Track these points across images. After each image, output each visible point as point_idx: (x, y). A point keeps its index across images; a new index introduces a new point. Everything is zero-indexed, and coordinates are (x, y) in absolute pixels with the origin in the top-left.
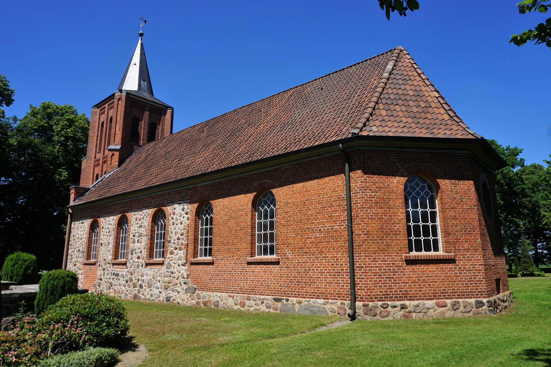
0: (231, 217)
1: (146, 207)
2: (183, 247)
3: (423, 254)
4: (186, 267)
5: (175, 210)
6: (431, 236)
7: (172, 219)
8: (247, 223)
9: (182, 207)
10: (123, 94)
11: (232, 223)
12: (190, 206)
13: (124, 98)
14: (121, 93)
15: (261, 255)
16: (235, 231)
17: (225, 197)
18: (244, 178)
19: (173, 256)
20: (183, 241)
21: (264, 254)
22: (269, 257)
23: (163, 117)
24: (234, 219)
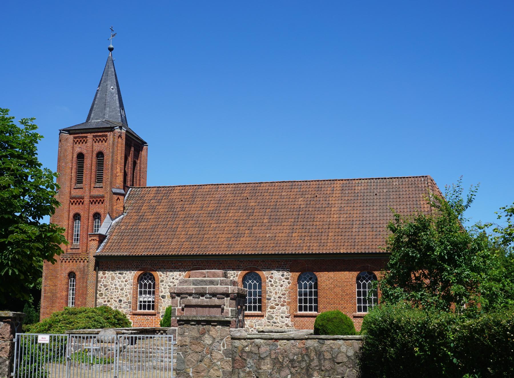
0: (337, 286)
1: (232, 269)
2: (285, 304)
3: (147, 311)
4: (290, 319)
5: (273, 275)
6: (362, 296)
7: (270, 281)
8: (353, 291)
9: (281, 273)
10: (123, 131)
11: (338, 290)
12: (291, 274)
13: (124, 136)
14: (121, 130)
15: (361, 311)
16: (341, 295)
17: (330, 271)
18: (348, 260)
19: (274, 310)
20: (286, 300)
21: (309, 311)
22: (151, 311)
23: (141, 152)
24: (340, 287)
